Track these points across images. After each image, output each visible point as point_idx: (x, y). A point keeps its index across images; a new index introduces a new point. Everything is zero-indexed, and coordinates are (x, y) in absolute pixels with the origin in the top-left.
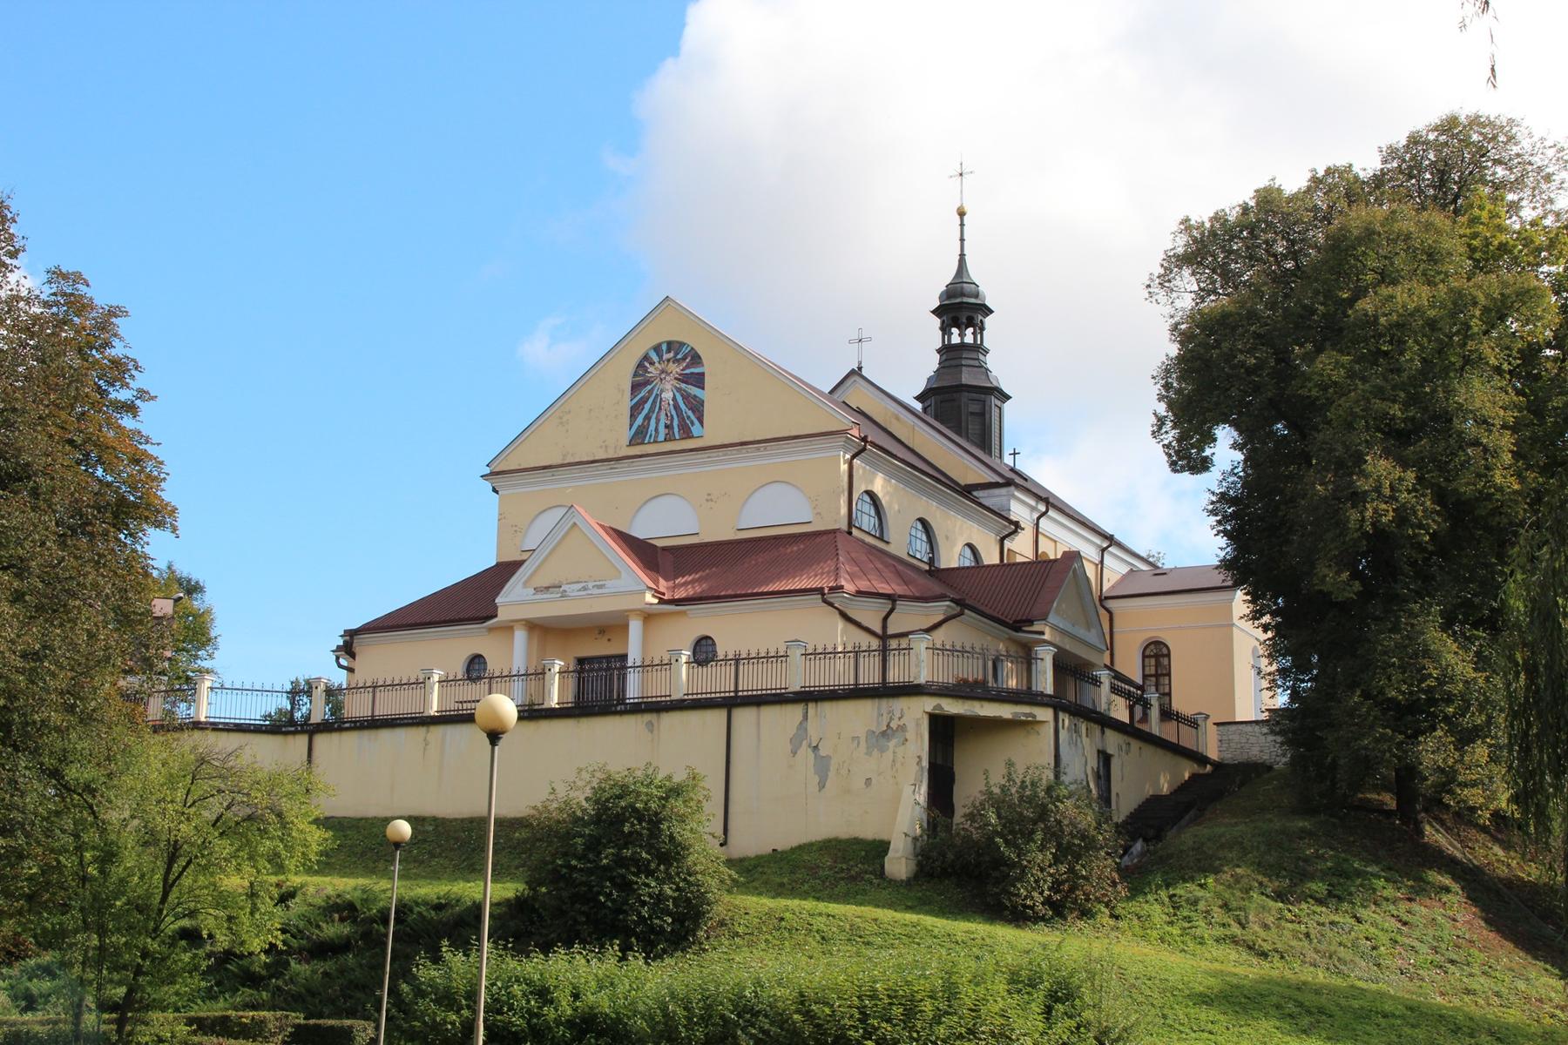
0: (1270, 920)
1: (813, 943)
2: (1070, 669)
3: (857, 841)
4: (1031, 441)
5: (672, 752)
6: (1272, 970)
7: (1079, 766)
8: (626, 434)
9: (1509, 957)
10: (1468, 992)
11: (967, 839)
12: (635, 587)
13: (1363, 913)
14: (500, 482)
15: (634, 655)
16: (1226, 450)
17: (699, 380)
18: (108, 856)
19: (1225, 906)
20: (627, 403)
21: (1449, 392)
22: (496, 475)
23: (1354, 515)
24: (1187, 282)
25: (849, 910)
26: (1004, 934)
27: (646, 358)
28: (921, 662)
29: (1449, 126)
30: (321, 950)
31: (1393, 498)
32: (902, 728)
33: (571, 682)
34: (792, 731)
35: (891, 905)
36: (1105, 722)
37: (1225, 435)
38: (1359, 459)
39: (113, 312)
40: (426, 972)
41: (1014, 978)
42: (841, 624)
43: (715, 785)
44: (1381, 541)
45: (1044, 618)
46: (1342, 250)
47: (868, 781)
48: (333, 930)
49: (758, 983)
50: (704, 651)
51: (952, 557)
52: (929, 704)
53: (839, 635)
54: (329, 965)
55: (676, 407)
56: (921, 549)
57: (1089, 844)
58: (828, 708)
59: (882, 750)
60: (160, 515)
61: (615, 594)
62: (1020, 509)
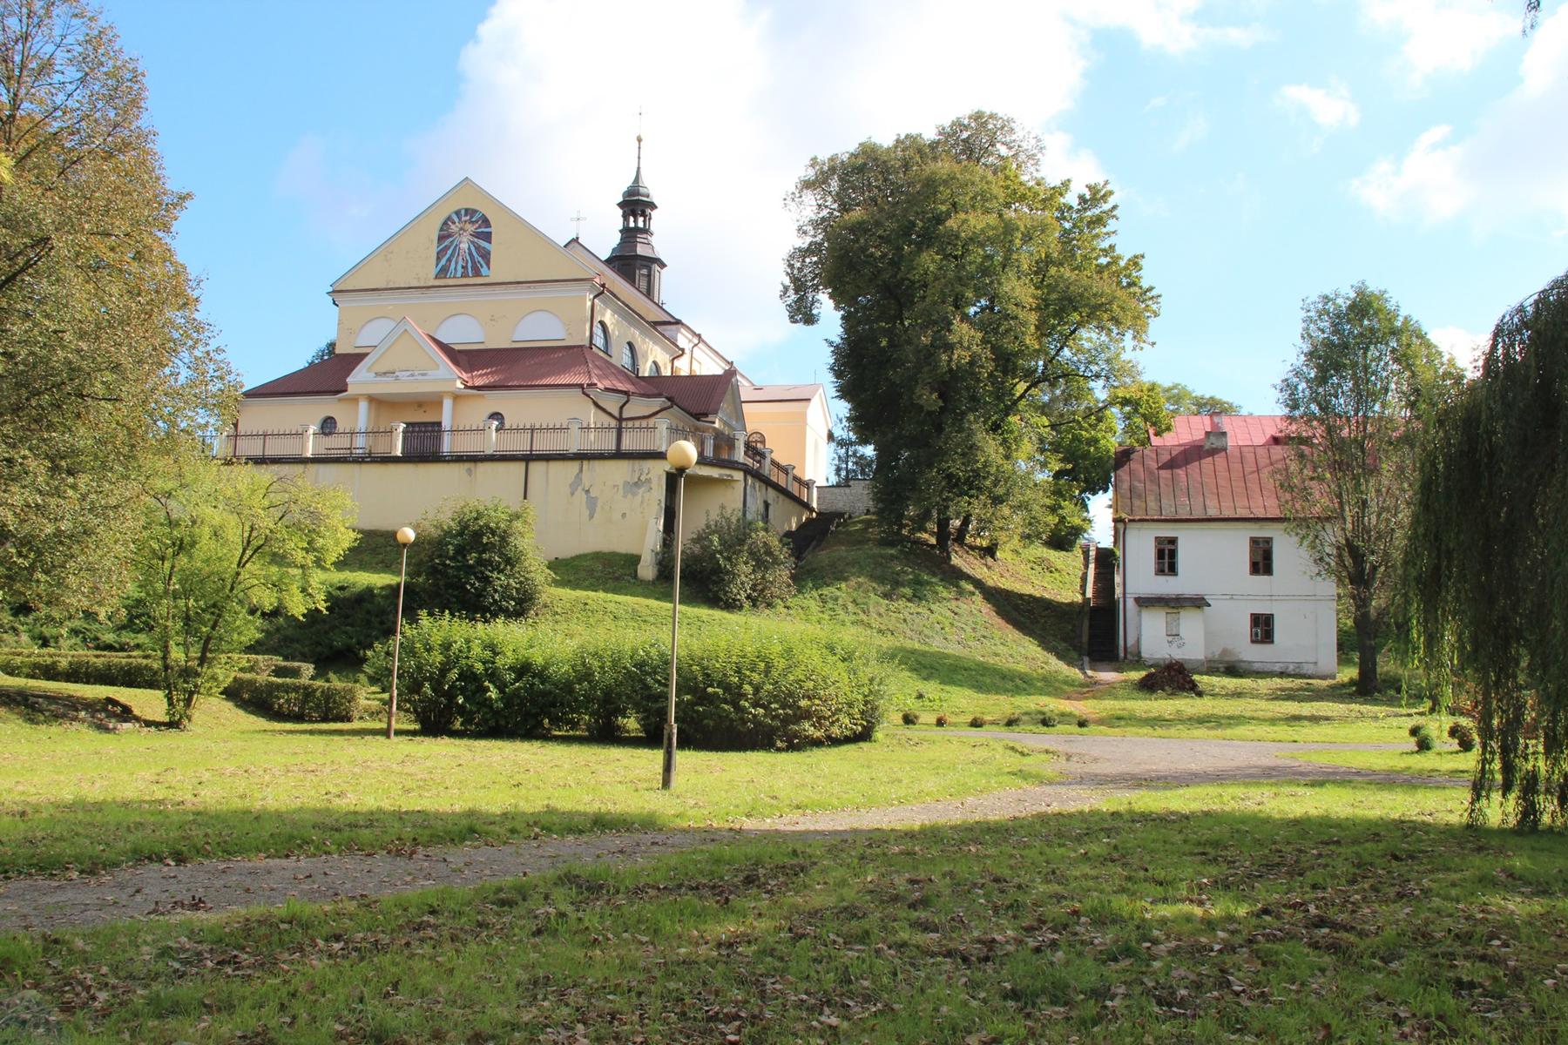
0: (882, 611)
1: (608, 620)
3: (614, 554)
5: (489, 493)
8: (434, 271)
9: (1012, 634)
10: (996, 655)
12: (452, 378)
15: (446, 424)
16: (830, 317)
17: (487, 237)
19: (854, 601)
20: (434, 250)
22: (337, 293)
23: (944, 357)
24: (810, 199)
27: (449, 218)
29: (977, 116)
31: (969, 348)
32: (649, 481)
42: (593, 409)
44: (956, 375)
45: (716, 413)
47: (624, 515)
50: (328, 426)
51: (646, 370)
53: (592, 416)
55: (470, 254)
56: (626, 360)
58: (597, 464)
59: (634, 494)
61: (435, 380)
62: (683, 340)
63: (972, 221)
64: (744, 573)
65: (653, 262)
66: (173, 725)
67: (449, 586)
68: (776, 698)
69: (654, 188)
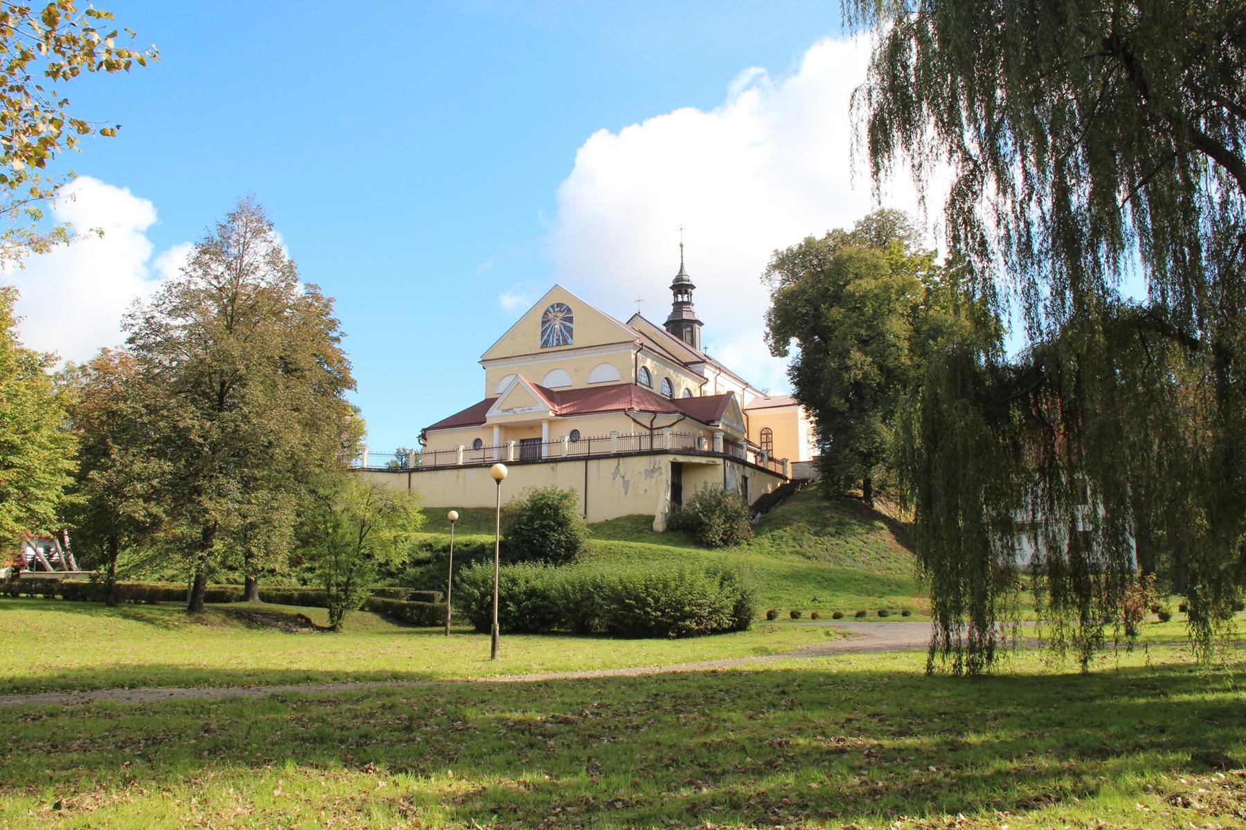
2: (730, 442)
3: (641, 516)
4: (708, 340)
6: (812, 564)
7: (734, 482)
8: (540, 344)
11: (688, 514)
12: (548, 410)
13: (849, 540)
14: (486, 364)
16: (794, 347)
17: (570, 320)
18: (336, 526)
19: (794, 539)
20: (540, 330)
21: (883, 324)
23: (846, 376)
24: (777, 276)
25: (638, 545)
26: (703, 553)
27: (548, 310)
28: (667, 440)
30: (418, 563)
33: (518, 449)
34: (613, 470)
35: (655, 542)
36: (745, 464)
37: (794, 341)
38: (848, 352)
39: (330, 300)
40: (465, 572)
41: (707, 572)
42: (633, 424)
43: (581, 493)
44: (857, 386)
45: (719, 420)
46: (839, 264)
48: (424, 555)
49: (602, 576)
50: (575, 436)
51: (680, 394)
52: (671, 458)
53: (633, 429)
54: (422, 569)
56: (666, 391)
57: (739, 515)
58: (628, 460)
60: (349, 383)
63: (864, 285)
64: (718, 524)
65: (693, 322)
66: (332, 629)
67: (524, 542)
68: (670, 606)
69: (692, 276)
